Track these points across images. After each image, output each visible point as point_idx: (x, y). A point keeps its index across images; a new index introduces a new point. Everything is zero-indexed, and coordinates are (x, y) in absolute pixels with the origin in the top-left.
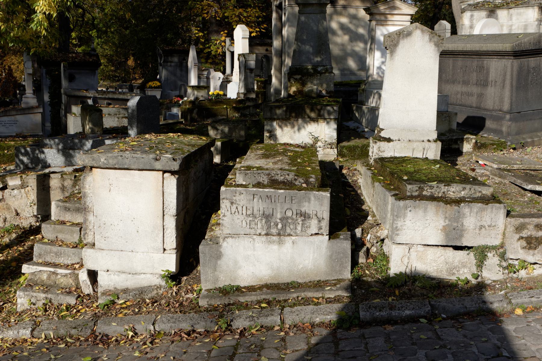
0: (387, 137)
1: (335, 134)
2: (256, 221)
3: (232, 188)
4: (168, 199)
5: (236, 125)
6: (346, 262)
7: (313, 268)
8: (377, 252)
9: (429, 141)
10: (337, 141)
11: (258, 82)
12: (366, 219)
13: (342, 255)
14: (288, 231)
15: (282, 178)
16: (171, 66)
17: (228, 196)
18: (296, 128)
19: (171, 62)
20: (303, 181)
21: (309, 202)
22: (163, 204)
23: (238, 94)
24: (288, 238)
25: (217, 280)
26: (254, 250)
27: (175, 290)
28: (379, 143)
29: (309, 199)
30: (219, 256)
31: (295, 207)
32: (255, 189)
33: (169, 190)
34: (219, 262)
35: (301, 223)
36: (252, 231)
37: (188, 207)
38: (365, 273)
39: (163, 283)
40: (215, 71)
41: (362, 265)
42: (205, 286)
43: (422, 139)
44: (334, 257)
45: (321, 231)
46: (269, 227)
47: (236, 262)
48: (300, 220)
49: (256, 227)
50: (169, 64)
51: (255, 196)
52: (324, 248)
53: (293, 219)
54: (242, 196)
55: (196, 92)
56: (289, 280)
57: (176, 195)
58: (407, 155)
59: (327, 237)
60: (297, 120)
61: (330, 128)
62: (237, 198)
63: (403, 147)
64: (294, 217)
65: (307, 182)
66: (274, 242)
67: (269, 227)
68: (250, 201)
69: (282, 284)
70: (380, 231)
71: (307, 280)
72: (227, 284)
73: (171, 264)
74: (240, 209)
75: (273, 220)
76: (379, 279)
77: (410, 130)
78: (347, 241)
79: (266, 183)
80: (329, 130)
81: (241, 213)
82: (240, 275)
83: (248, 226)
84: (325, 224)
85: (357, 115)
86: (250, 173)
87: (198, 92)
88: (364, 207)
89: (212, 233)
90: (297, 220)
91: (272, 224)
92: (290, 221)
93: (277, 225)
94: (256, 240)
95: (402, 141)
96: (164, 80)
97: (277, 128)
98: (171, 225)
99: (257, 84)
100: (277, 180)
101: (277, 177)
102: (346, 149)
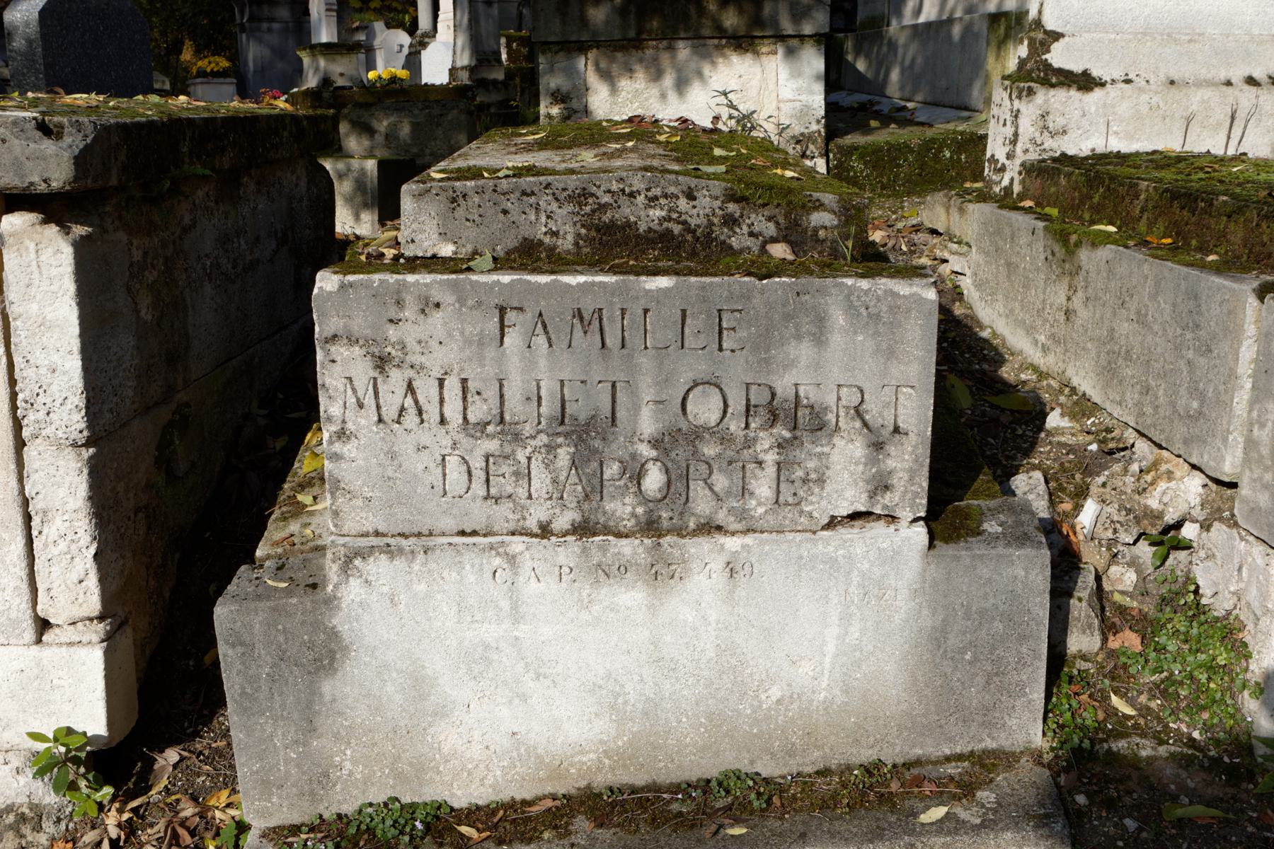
0: (1077, 68)
1: (817, 100)
2: (521, 456)
3: (376, 277)
4: (39, 357)
5: (437, 111)
6: (1022, 663)
7: (840, 699)
8: (1142, 591)
9: (1251, 81)
10: (827, 126)
11: (510, 40)
12: (1041, 427)
13: (998, 626)
14: (702, 504)
15: (657, 213)
16: (269, 30)
17: (359, 324)
18: (668, 80)
19: (271, 20)
20: (770, 229)
21: (820, 339)
22: (12, 382)
23: (453, 71)
24: (700, 547)
25: (323, 778)
26: (516, 616)
27: (114, 832)
28: (1043, 97)
29: (821, 321)
30: (326, 654)
31: (736, 372)
32: (506, 278)
33: (34, 307)
34: (327, 687)
35: (771, 458)
36: (503, 515)
37: (182, 397)
38: (1112, 712)
39: (47, 796)
40: (389, 26)
41: (1083, 665)
42: (261, 814)
43: (1223, 75)
44: (953, 641)
45: (888, 499)
46: (595, 489)
47: (419, 685)
48: (765, 442)
49: (522, 492)
50: (265, 25)
51: (511, 316)
52: (904, 593)
53: (725, 439)
54: (437, 316)
55: (322, 63)
56: (711, 768)
57: (75, 330)
58: (1160, 147)
59: (920, 531)
60: (670, 48)
61: (796, 74)
62: (410, 330)
63: (1144, 109)
64: (735, 426)
65: (793, 234)
66: (624, 569)
67: (595, 489)
68: (481, 344)
69: (675, 788)
70: (1162, 485)
71: (808, 763)
72: (378, 795)
73: (77, 692)
74: (426, 390)
75: (618, 448)
76: (1192, 742)
77: (1170, 37)
78: (1028, 551)
79: (566, 244)
80: (793, 84)
81: (432, 413)
82: (446, 749)
83: (479, 488)
84: (909, 463)
85: (861, 66)
86: (480, 192)
87: (327, 60)
88: (1007, 373)
89: (294, 527)
90: (749, 443)
91: (612, 470)
92: (710, 450)
93: (638, 477)
94: (527, 564)
95: (1140, 82)
96: (255, 72)
97: (592, 78)
98: (62, 492)
99: (508, 46)
100: (628, 224)
101: (626, 212)
102: (861, 157)
